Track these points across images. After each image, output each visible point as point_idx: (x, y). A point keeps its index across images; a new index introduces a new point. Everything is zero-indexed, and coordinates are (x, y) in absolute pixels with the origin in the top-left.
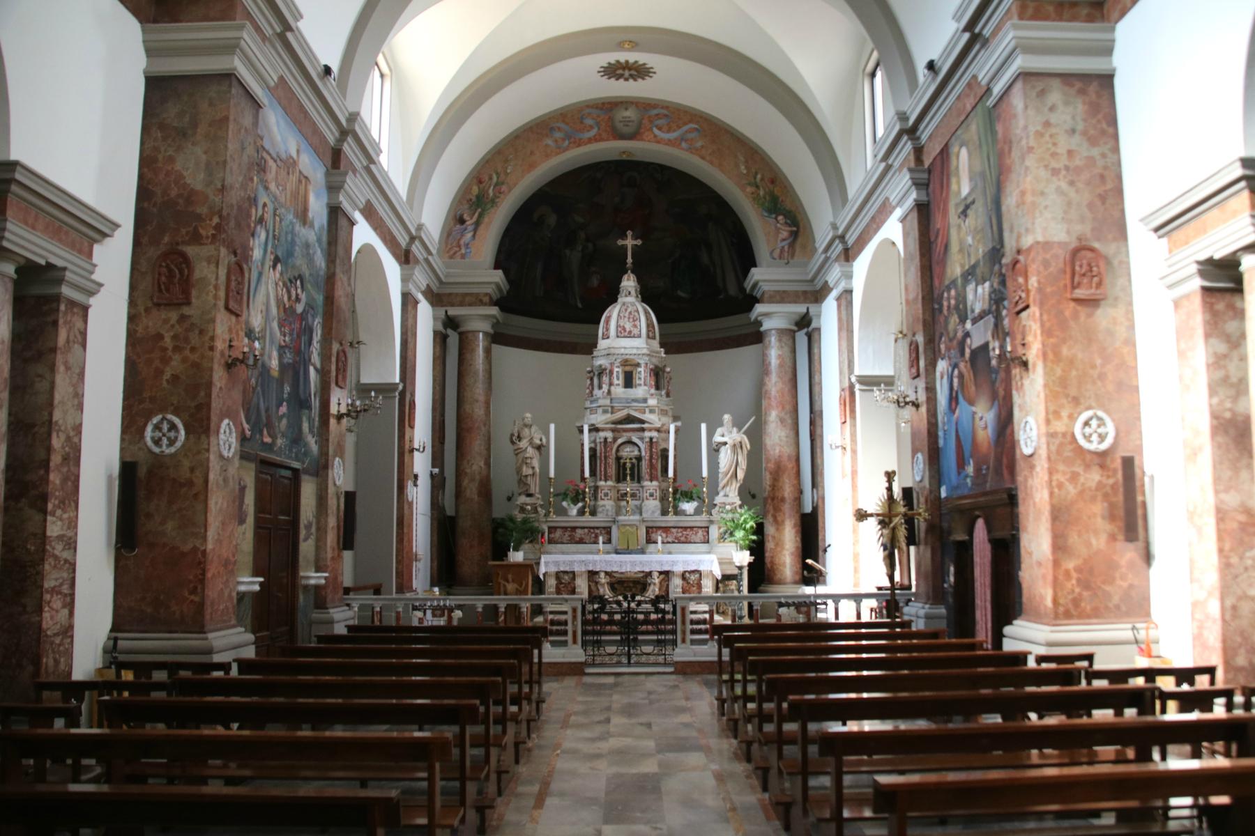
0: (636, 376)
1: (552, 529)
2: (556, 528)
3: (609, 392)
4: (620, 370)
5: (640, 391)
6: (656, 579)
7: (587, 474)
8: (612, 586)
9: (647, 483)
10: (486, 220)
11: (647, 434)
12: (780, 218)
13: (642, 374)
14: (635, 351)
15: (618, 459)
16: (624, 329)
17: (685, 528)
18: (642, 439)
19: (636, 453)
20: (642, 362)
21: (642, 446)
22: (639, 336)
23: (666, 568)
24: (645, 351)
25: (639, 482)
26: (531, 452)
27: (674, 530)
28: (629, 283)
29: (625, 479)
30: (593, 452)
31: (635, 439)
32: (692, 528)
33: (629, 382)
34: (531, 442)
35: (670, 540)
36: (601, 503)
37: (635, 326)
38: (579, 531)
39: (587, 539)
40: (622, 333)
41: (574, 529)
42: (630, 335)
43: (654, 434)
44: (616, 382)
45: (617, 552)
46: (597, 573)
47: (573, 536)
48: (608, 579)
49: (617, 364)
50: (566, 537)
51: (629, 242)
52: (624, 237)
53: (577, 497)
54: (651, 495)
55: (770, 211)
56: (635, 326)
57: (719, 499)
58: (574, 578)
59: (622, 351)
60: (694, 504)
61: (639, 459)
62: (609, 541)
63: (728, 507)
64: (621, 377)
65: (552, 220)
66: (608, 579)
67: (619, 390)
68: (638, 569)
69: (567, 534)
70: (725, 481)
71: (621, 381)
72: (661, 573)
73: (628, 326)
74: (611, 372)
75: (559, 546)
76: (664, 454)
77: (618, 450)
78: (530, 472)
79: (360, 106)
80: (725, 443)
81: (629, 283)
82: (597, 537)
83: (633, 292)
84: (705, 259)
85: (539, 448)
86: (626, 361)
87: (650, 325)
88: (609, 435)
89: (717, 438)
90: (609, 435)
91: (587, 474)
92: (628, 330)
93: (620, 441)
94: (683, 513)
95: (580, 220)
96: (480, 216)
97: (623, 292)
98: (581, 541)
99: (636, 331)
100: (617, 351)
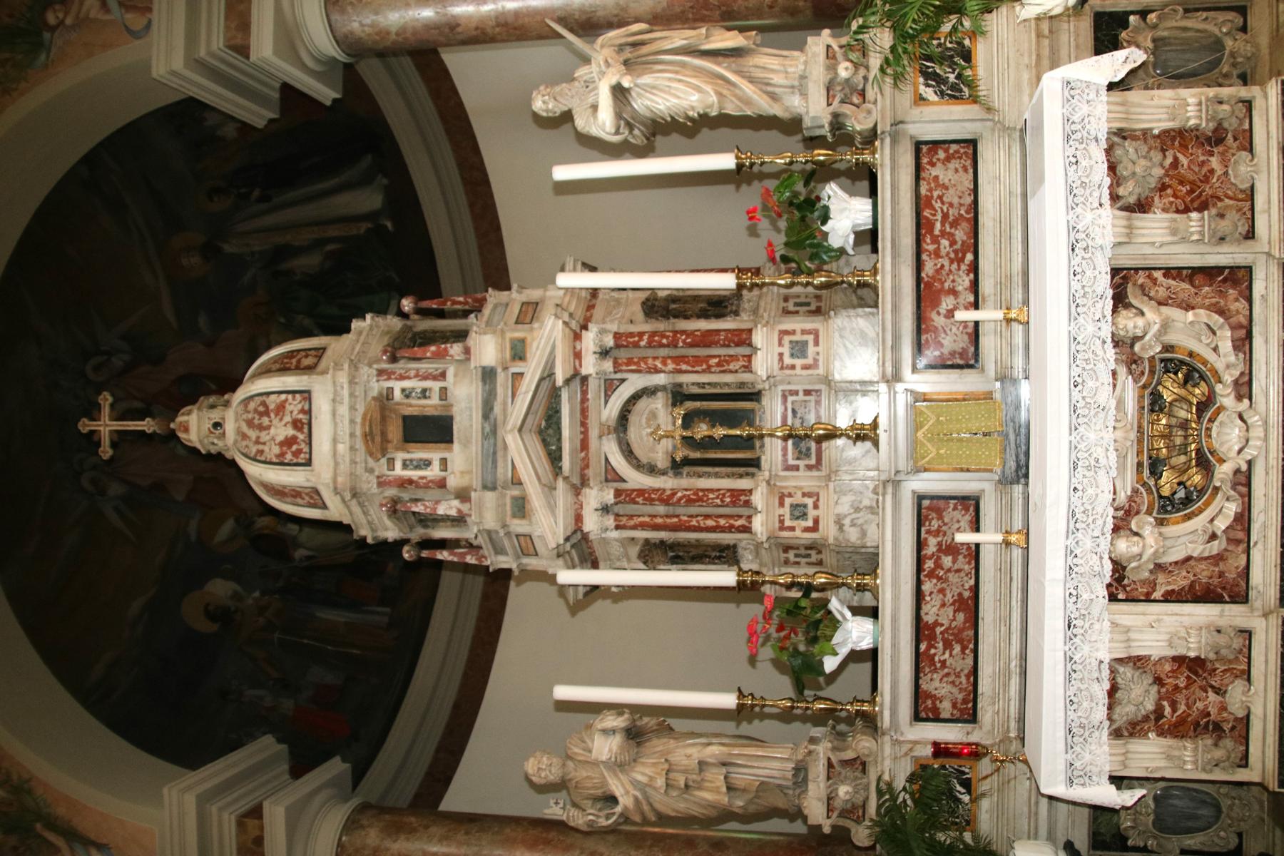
0: (417, 407)
1: (924, 709)
2: (918, 694)
3: (463, 495)
4: (400, 456)
5: (464, 396)
6: (1147, 321)
7: (725, 577)
8: (1172, 507)
9: (764, 364)
10: (61, 811)
11: (590, 366)
12: (51, 19)
13: (411, 387)
14: (344, 410)
15: (677, 466)
16: (289, 442)
17: (921, 226)
18: (610, 387)
19: (659, 404)
20: (376, 387)
21: (635, 382)
22: (307, 395)
23: (1103, 283)
24: (343, 378)
25: (755, 396)
26: (647, 771)
27: (929, 268)
28: (195, 426)
29: (748, 442)
30: (652, 554)
31: (611, 410)
32: (920, 204)
33: (433, 429)
34: (619, 766)
35: (964, 281)
36: (829, 531)
37: (281, 408)
38: (931, 612)
39: (959, 584)
40: (297, 451)
41: (922, 630)
42: (304, 424)
43: (590, 340)
44: (434, 472)
45: (1021, 473)
46: (1119, 568)
47: (951, 631)
48: (1145, 524)
49: (381, 467)
50: (957, 660)
51: (106, 426)
52: (92, 440)
53: (805, 619)
54: (799, 349)
55: (38, 46)
56: (281, 408)
57: (815, 110)
58: (1138, 662)
59: (341, 448)
60: (833, 193)
61: (678, 396)
62: (971, 505)
63: (844, 70)
64: (419, 453)
65: (220, 589)
66: (1145, 524)
67: (460, 461)
68: (1105, 396)
69: (939, 652)
70: (748, 89)
71: (434, 454)
72: (1120, 300)
73: (281, 431)
74: (405, 483)
75: (985, 685)
76: (660, 306)
77: (652, 470)
78: (716, 777)
79: (605, 568)
80: (620, 93)
81: (195, 426)
82: (952, 549)
83: (215, 415)
84: (309, 263)
85: (634, 735)
86: (368, 436)
87: (283, 366)
88: (595, 496)
89: (603, 123)
90: (595, 496)
91: (725, 577)
92: (310, 429)
93: (618, 462)
94: (869, 238)
95: (227, 527)
96: (52, 824)
97: (216, 445)
98: (970, 605)
99: (294, 406)
100: (344, 467)
